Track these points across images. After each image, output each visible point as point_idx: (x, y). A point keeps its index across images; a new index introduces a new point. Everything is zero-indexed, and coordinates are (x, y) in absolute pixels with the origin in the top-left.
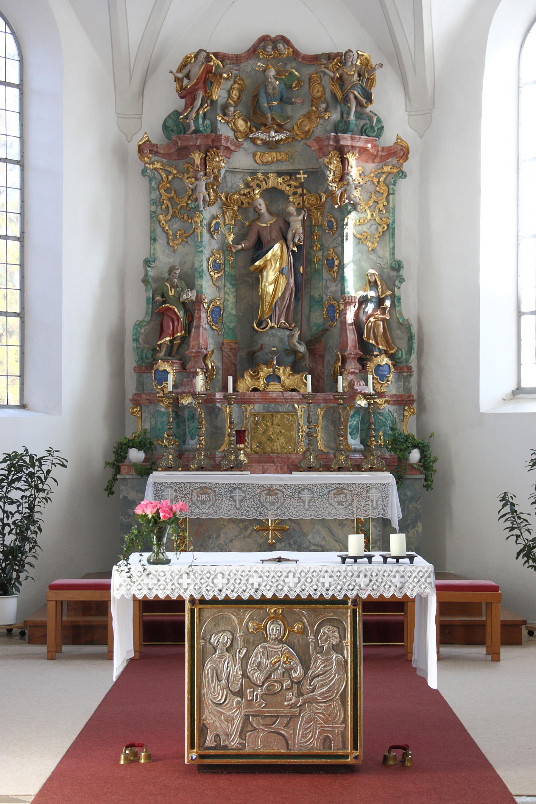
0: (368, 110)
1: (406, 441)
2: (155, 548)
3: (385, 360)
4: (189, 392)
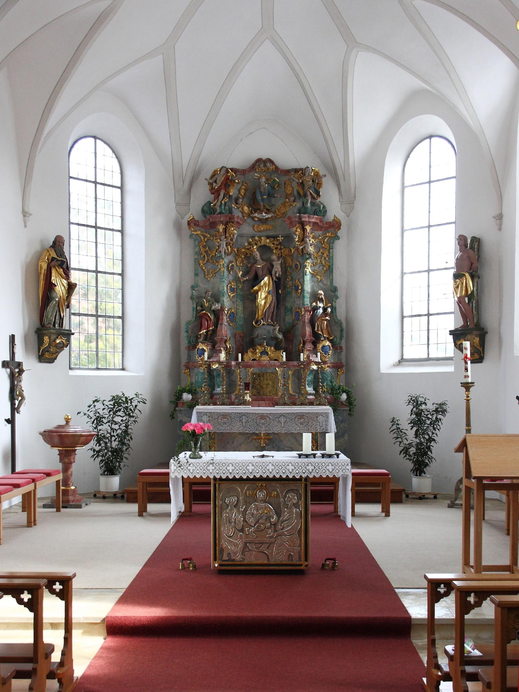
0: (318, 201)
1: (339, 388)
2: (193, 449)
3: (328, 343)
4: (217, 361)
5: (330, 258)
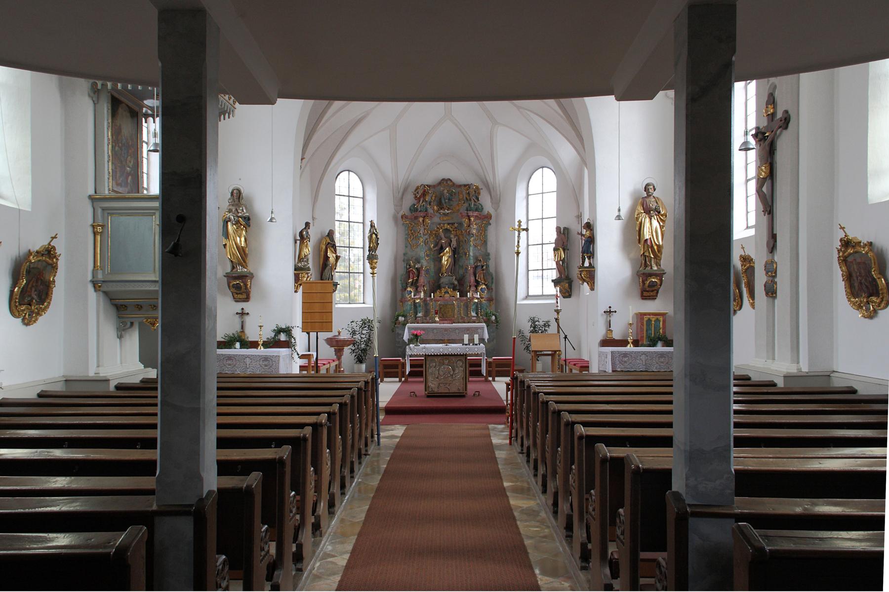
3: (484, 286)
5: (486, 236)
